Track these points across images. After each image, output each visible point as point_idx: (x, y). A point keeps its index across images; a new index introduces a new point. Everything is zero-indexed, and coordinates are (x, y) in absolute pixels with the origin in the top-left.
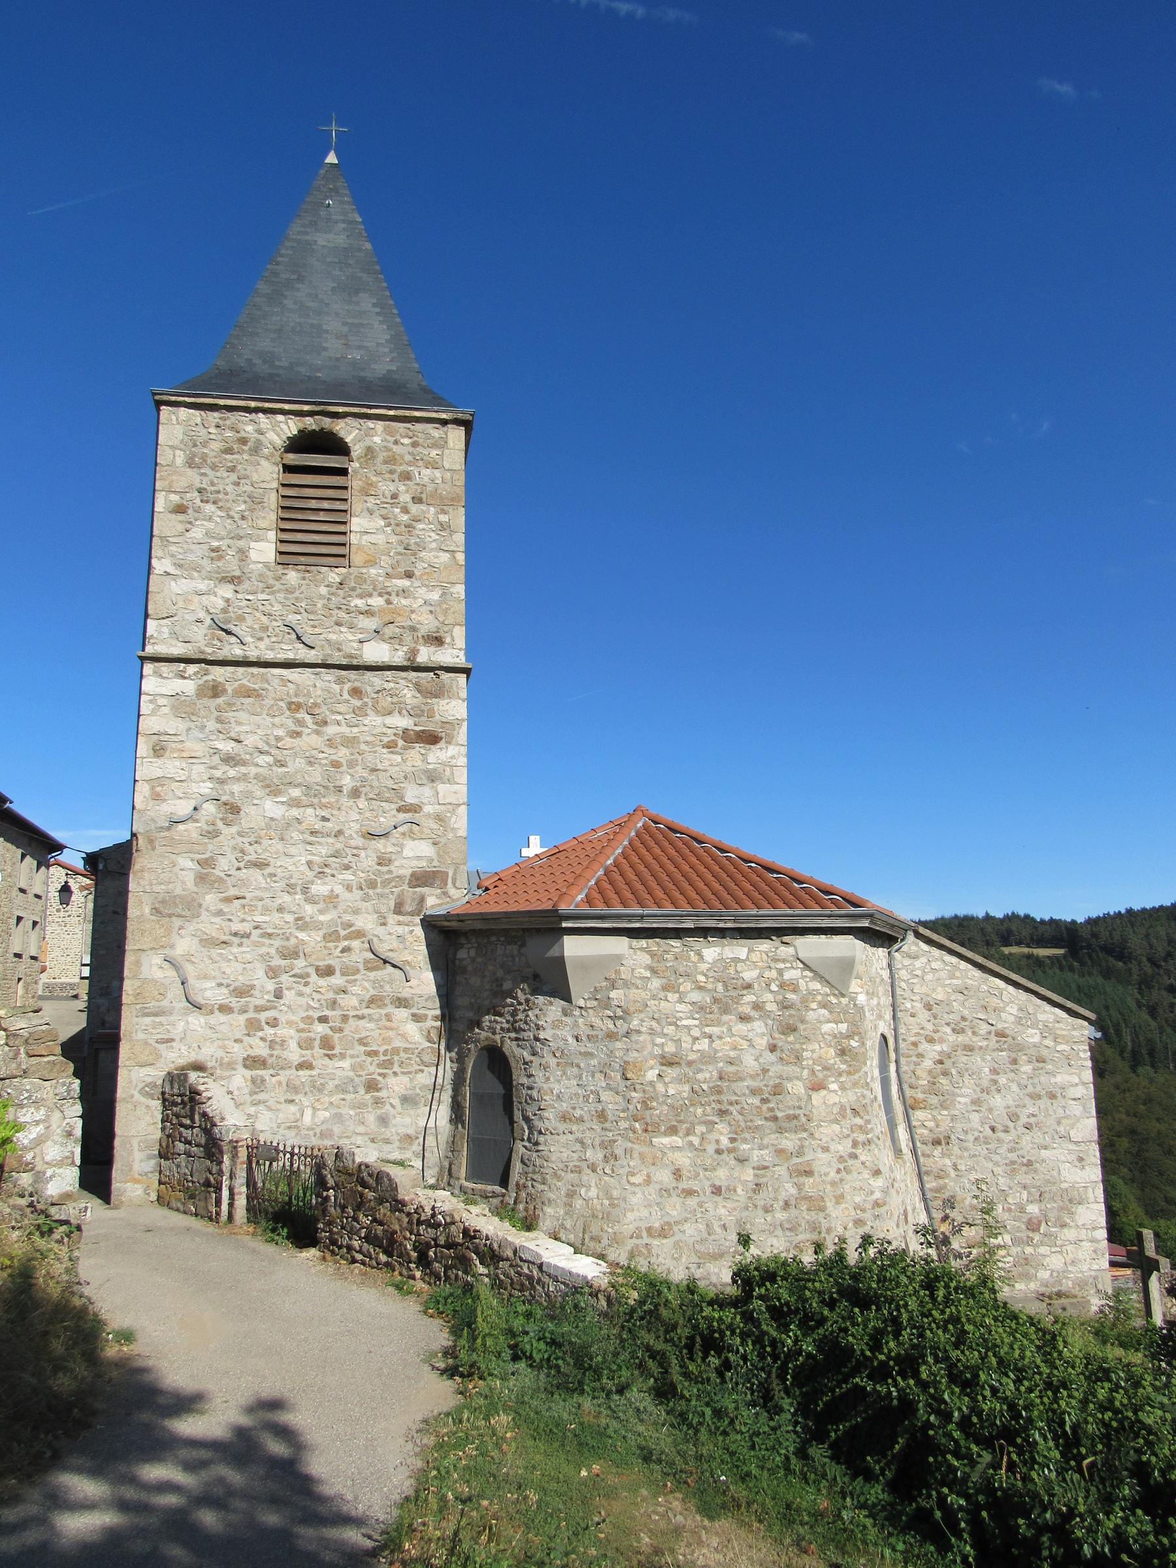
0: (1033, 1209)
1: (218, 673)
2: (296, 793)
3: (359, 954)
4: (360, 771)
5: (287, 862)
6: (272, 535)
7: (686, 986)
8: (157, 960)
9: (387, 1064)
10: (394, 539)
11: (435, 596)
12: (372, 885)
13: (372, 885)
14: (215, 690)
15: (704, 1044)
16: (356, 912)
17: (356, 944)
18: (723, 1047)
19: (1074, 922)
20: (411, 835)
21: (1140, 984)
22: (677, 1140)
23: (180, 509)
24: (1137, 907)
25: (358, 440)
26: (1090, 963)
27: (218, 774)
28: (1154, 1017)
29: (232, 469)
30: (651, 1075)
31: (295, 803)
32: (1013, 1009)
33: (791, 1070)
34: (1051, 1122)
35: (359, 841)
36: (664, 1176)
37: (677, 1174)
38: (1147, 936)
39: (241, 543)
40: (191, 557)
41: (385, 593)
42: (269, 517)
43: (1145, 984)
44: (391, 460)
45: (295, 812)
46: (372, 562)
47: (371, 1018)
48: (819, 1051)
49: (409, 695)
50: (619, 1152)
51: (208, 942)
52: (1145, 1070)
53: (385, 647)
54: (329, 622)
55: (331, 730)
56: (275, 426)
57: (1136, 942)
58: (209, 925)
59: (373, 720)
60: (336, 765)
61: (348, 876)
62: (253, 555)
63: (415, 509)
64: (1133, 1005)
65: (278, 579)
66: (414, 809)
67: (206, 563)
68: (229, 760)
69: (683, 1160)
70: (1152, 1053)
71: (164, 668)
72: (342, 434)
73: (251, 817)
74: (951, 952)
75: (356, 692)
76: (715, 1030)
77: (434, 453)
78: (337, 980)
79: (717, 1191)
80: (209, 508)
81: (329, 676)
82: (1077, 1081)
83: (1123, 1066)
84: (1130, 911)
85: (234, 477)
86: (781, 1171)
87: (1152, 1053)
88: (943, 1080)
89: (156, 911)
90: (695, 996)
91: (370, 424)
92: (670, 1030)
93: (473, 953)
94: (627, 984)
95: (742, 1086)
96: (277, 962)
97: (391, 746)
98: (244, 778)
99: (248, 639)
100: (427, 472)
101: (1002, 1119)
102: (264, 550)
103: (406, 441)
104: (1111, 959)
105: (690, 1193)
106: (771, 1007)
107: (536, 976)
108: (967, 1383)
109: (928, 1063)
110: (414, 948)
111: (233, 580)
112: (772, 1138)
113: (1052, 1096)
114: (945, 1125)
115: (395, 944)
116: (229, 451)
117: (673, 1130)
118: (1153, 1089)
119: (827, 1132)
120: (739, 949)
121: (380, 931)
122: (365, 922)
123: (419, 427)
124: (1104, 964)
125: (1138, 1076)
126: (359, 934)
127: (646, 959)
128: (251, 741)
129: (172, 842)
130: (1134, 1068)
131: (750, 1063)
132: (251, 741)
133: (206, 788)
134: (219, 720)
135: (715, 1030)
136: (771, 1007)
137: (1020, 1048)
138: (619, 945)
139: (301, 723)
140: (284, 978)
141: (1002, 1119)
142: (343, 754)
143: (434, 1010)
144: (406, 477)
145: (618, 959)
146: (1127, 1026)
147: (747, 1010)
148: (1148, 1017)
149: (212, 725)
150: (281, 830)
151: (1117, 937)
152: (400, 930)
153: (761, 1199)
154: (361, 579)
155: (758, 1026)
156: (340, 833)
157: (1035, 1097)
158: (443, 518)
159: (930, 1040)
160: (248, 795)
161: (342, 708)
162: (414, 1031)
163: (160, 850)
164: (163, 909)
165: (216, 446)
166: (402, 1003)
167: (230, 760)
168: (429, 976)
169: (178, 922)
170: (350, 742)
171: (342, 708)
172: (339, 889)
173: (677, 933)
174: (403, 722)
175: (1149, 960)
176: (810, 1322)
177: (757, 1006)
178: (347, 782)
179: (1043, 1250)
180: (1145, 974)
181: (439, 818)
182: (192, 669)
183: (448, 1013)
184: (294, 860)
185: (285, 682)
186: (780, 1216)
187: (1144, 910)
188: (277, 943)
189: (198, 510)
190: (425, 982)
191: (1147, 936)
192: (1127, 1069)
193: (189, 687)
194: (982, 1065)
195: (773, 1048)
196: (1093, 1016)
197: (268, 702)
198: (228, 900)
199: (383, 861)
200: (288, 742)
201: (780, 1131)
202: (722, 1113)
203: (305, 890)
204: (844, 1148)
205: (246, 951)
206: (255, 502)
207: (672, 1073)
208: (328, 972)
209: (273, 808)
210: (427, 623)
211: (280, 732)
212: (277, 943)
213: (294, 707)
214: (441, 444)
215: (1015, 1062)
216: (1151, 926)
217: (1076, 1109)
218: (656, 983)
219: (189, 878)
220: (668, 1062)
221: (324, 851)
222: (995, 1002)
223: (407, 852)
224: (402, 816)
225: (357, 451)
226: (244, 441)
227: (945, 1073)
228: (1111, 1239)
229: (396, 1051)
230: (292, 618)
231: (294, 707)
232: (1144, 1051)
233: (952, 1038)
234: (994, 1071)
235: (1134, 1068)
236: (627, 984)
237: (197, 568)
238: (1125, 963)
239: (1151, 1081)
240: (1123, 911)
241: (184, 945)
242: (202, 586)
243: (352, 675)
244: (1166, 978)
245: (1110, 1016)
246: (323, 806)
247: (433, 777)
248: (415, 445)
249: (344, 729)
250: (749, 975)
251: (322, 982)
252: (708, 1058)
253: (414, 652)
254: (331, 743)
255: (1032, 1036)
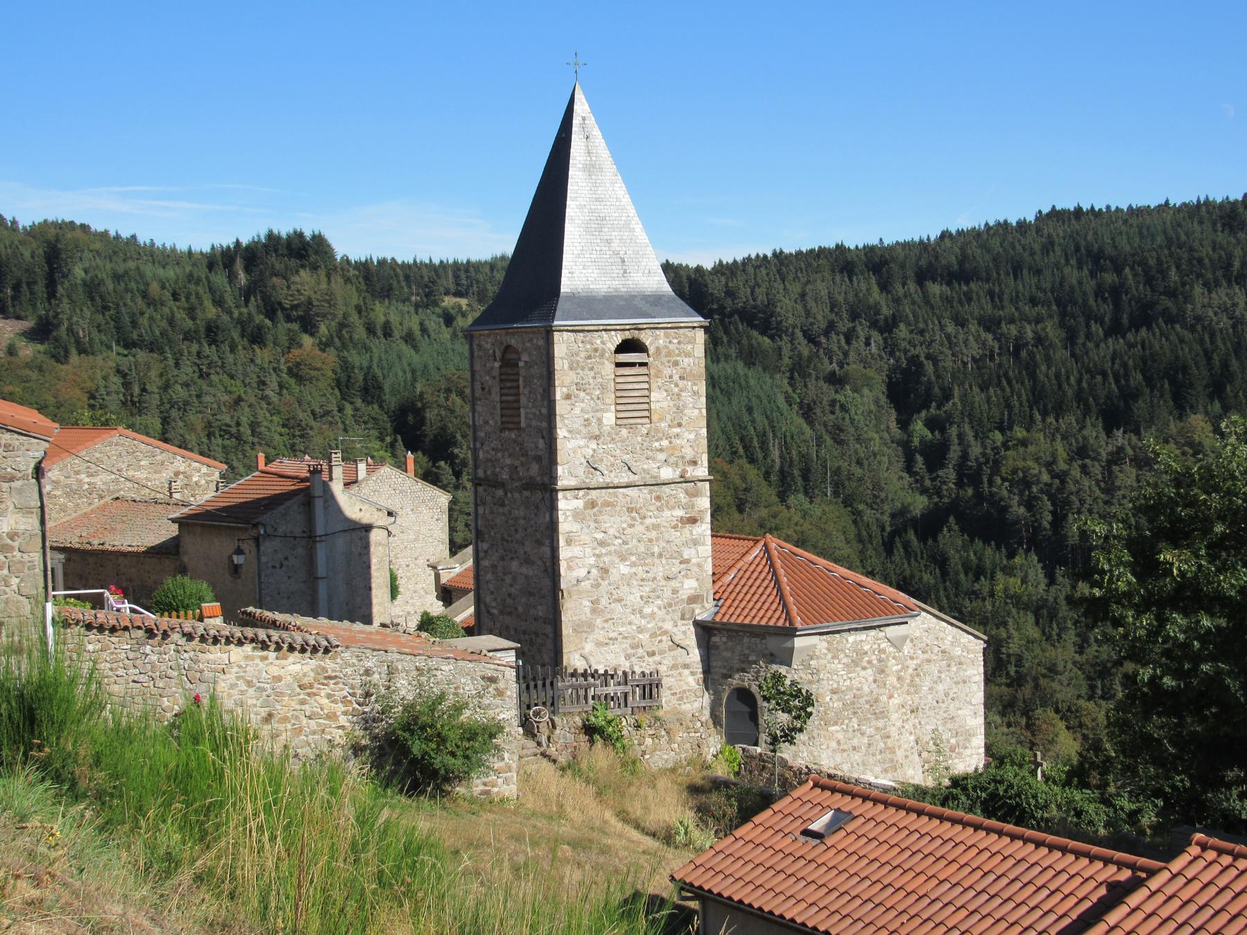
0: (953, 741)
1: (594, 494)
2: (633, 558)
3: (666, 643)
4: (663, 544)
5: (631, 598)
6: (613, 407)
7: (842, 656)
8: (577, 656)
9: (681, 699)
10: (671, 404)
11: (692, 436)
12: (670, 605)
13: (670, 605)
14: (593, 504)
15: (848, 683)
16: (663, 621)
17: (664, 638)
18: (855, 683)
19: (699, 269)
20: (686, 576)
21: (792, 371)
22: (837, 728)
23: (568, 397)
24: (789, 249)
25: (651, 343)
26: (725, 339)
27: (597, 552)
28: (811, 423)
29: (592, 369)
30: (828, 699)
31: (633, 565)
32: (950, 638)
33: (882, 690)
34: (963, 696)
35: (663, 582)
36: (833, 744)
37: (839, 743)
38: (803, 295)
39: (599, 414)
40: (576, 426)
41: (668, 437)
42: (610, 398)
43: (798, 370)
44: (669, 354)
45: (634, 570)
46: (661, 419)
47: (672, 676)
48: (892, 680)
49: (682, 496)
50: (815, 735)
51: (599, 644)
52: (797, 499)
53: (670, 469)
54: (643, 458)
55: (648, 521)
56: (611, 337)
57: (788, 309)
58: (599, 635)
59: (667, 513)
60: (650, 540)
61: (659, 602)
62: (605, 421)
63: (681, 383)
64: (781, 400)
65: (617, 434)
66: (687, 561)
67: (582, 428)
68: (602, 544)
69: (840, 736)
70: (806, 474)
71: (568, 494)
72: (644, 340)
73: (614, 575)
74: (952, 624)
75: (658, 498)
76: (852, 675)
77: (690, 347)
78: (657, 658)
79: (854, 749)
80: (582, 394)
81: (645, 490)
82: (976, 672)
83: (768, 493)
84: (778, 255)
85: (592, 374)
86: (878, 737)
87: (806, 474)
88: (917, 679)
89: (574, 630)
90: (845, 660)
91: (658, 332)
92: (835, 677)
93: (724, 639)
94: (818, 658)
95: (862, 701)
96: (630, 651)
97: (675, 527)
98: (609, 553)
99: (605, 472)
100: (686, 360)
101: (941, 696)
102: (609, 418)
103: (675, 341)
104: (755, 333)
105: (844, 750)
106: (875, 662)
107: (772, 655)
108: (1035, 797)
109: (910, 671)
110: (691, 640)
111: (597, 438)
112: (874, 723)
113: (965, 682)
114: (917, 701)
115: (682, 636)
116: (589, 357)
117: (836, 723)
118: (806, 526)
119: (894, 716)
120: (862, 636)
121: (675, 630)
122: (668, 626)
123: (681, 331)
124: (745, 341)
125: (788, 508)
126: (665, 632)
127: (825, 644)
128: (611, 532)
129: (579, 592)
130: (783, 497)
131: (866, 689)
132: (611, 532)
133: (592, 560)
134: (596, 521)
135: (852, 675)
136: (875, 662)
137: (951, 658)
138: (815, 639)
139: (634, 519)
140: (633, 659)
141: (941, 696)
142: (653, 534)
143: (699, 668)
144: (676, 364)
145: (815, 646)
146: (775, 436)
147: (865, 664)
148: (800, 421)
149: (593, 525)
150: (627, 580)
151: (761, 298)
152: (683, 628)
153: (872, 750)
154: (657, 430)
155: (869, 671)
156: (655, 578)
157: (957, 683)
158: (695, 388)
159: (912, 658)
160: (612, 563)
161: (652, 508)
162: (691, 680)
163: (575, 597)
164: (579, 629)
165: (583, 355)
166: (686, 666)
167: (602, 544)
168: (697, 651)
169: (585, 635)
170: (656, 527)
171: (652, 508)
172: (656, 610)
173: (838, 632)
174: (680, 513)
175: (805, 334)
176: (983, 789)
177: (869, 662)
178: (656, 550)
179: (956, 761)
180: (800, 356)
181: (699, 565)
182: (581, 493)
183: (707, 671)
184: (634, 598)
185: (625, 496)
186: (879, 757)
187: (799, 253)
188: (629, 641)
189: (577, 396)
190: (695, 655)
191: (803, 295)
192: (775, 499)
193: (580, 504)
194: (934, 668)
195: (875, 681)
196: (986, 638)
197: (618, 508)
198: (607, 621)
199: (675, 592)
200: (629, 531)
201: (877, 719)
202: (855, 713)
203: (641, 612)
204: (899, 724)
205: (615, 647)
206: (603, 387)
207: (835, 697)
208: (652, 654)
209: (624, 569)
210: (689, 453)
211: (625, 525)
212: (629, 641)
213: (630, 510)
214: (692, 341)
215: (949, 666)
216: (808, 282)
217: (974, 687)
218: (830, 656)
219: (587, 610)
220: (834, 692)
221: (647, 589)
222: (942, 635)
223: (686, 586)
224: (683, 566)
225: (652, 350)
226: (596, 350)
227: (918, 675)
228: (986, 755)
229: (684, 691)
230: (626, 457)
231: (630, 510)
232: (796, 472)
233: (921, 656)
234: (940, 672)
235: (783, 497)
236: (818, 658)
237: (579, 432)
238: (772, 338)
239: (805, 515)
240: (769, 255)
241: (589, 647)
242: (582, 443)
243: (655, 488)
244: (826, 360)
245: (753, 421)
246: (646, 565)
247: (696, 543)
248: (679, 343)
249: (653, 520)
250: (866, 648)
251: (651, 660)
252: (850, 688)
253: (684, 471)
254: (648, 528)
255: (958, 651)
